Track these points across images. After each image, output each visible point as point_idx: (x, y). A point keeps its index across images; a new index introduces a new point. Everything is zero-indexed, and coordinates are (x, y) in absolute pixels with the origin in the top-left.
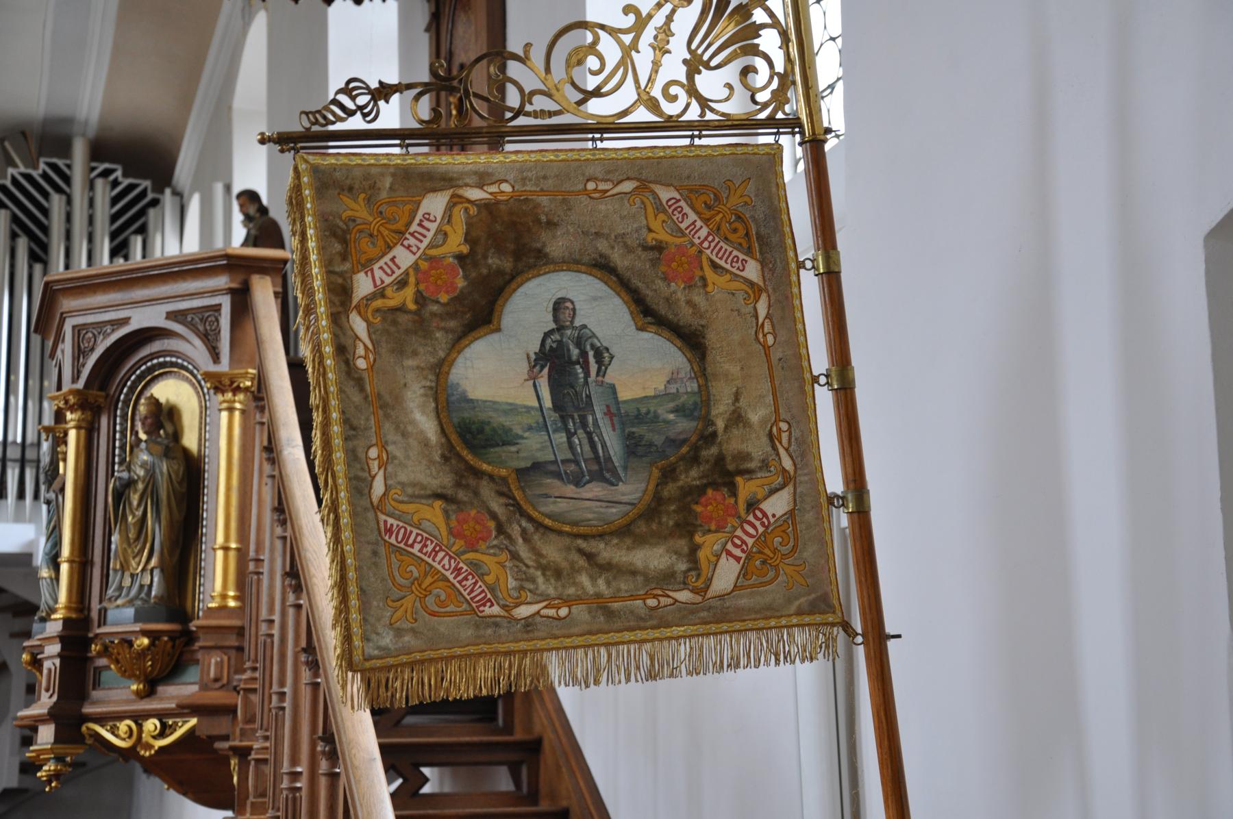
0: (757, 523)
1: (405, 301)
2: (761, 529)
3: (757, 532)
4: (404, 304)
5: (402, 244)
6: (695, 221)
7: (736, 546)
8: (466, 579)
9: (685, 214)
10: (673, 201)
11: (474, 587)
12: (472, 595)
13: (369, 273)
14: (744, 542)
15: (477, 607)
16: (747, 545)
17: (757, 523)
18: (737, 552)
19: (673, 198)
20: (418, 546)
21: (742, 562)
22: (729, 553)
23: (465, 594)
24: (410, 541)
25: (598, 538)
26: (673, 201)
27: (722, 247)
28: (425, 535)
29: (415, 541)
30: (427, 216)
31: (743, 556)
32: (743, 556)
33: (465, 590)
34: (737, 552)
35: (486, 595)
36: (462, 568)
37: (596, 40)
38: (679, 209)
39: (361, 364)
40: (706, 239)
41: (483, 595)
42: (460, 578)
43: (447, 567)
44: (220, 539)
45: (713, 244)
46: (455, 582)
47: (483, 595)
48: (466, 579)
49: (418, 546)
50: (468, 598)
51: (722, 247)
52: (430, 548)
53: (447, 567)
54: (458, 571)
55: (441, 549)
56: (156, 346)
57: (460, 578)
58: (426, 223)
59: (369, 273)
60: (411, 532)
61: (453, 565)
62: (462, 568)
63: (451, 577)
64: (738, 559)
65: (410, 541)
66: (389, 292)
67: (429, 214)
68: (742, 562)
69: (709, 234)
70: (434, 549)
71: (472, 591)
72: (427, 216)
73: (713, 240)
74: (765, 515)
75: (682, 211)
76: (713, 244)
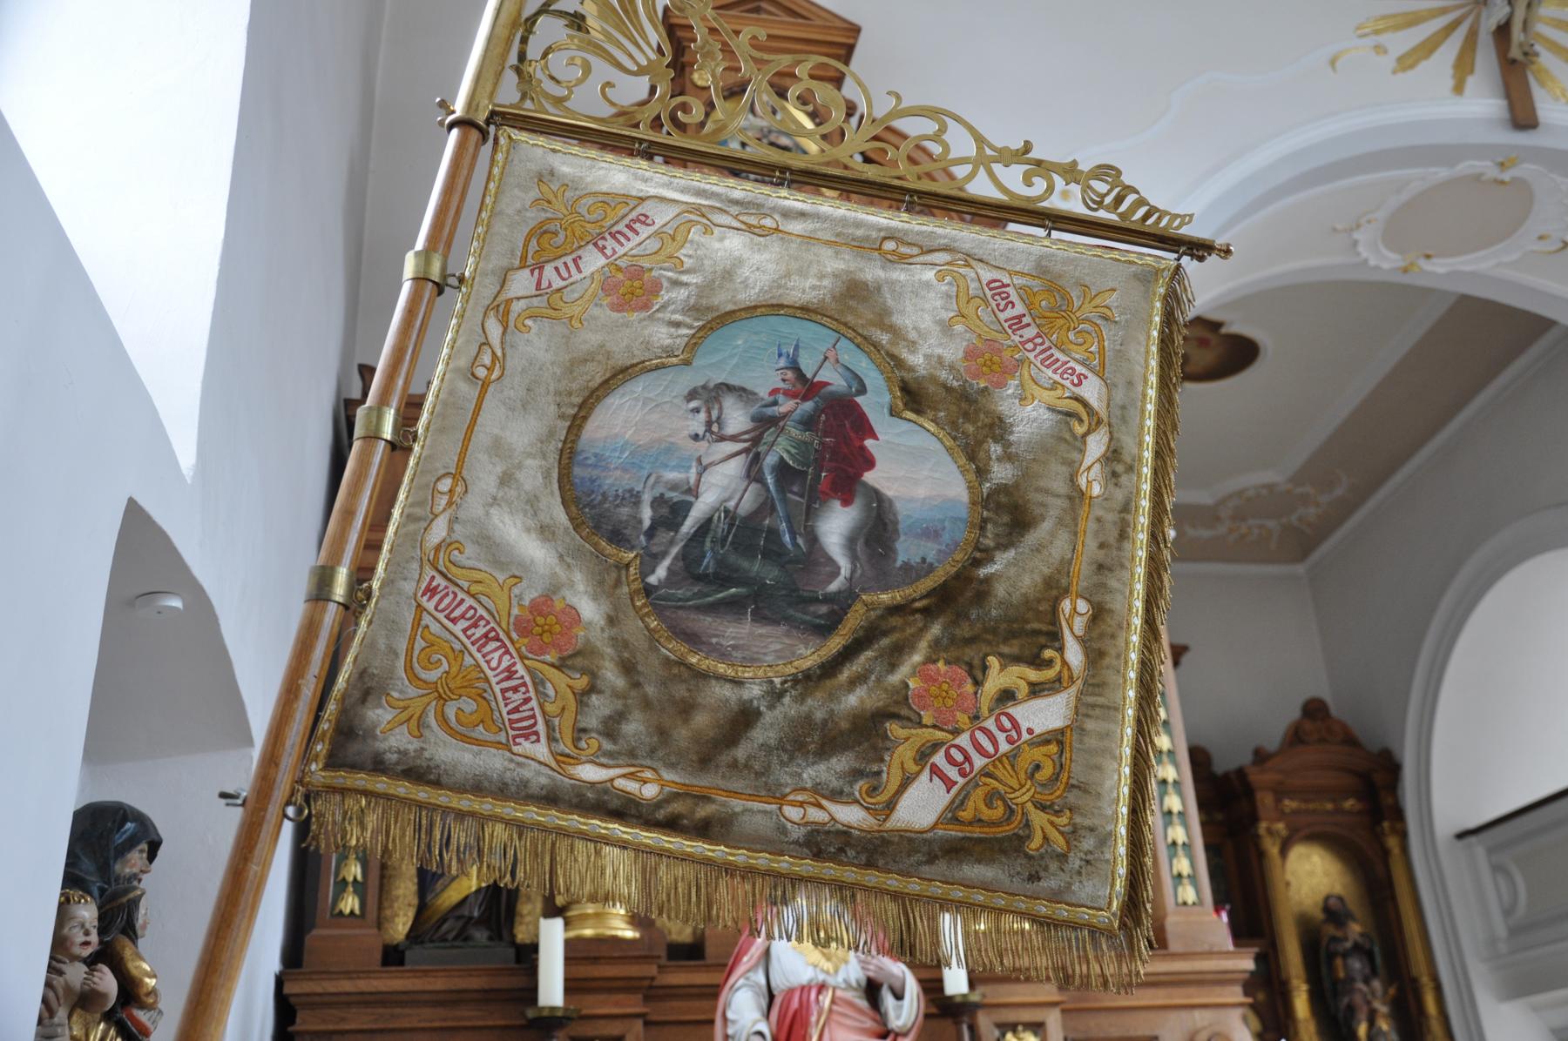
0: (1001, 737)
1: (1002, 670)
2: (1004, 747)
3: (997, 750)
4: (1003, 668)
5: (595, 244)
6: (1024, 315)
7: (951, 761)
8: (515, 689)
9: (1012, 302)
10: (997, 284)
11: (521, 705)
12: (515, 716)
13: (536, 272)
14: (967, 758)
15: (515, 737)
16: (971, 765)
17: (1001, 737)
18: (952, 773)
19: (999, 281)
20: (463, 624)
21: (954, 790)
22: (936, 771)
23: (504, 711)
24: (457, 613)
25: (385, 881)
26: (997, 284)
27: (1052, 355)
28: (481, 611)
29: (462, 616)
30: (643, 218)
31: (961, 781)
32: (961, 781)
33: (506, 705)
34: (952, 773)
35: (535, 724)
36: (516, 672)
37: (943, 129)
38: (1004, 295)
40: (1030, 340)
41: (531, 722)
42: (506, 685)
43: (494, 664)
45: (1039, 348)
46: (497, 689)
47: (531, 722)
48: (515, 689)
49: (463, 624)
50: (506, 717)
51: (1052, 355)
52: (479, 632)
53: (494, 664)
54: (510, 673)
55: (497, 639)
57: (506, 685)
58: (637, 226)
59: (536, 272)
60: (462, 601)
61: (504, 664)
62: (516, 672)
63: (494, 681)
64: (949, 784)
65: (457, 613)
66: (1023, 689)
67: (647, 217)
68: (954, 790)
69: (1038, 336)
70: (486, 635)
71: (516, 710)
72: (643, 218)
73: (1042, 344)
74: (1015, 725)
75: (1007, 298)
76: (1039, 348)
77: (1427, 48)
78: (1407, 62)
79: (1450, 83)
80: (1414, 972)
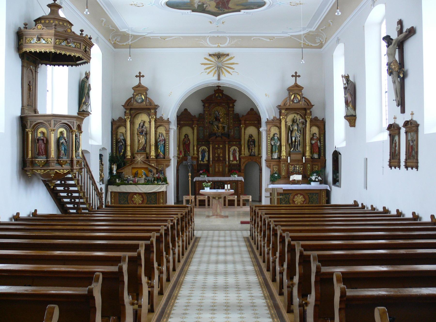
39: (45, 143)
44: (53, 151)
56: (40, 124)
77: (211, 71)
78: (208, 73)
79: (213, 75)
80: (242, 144)
